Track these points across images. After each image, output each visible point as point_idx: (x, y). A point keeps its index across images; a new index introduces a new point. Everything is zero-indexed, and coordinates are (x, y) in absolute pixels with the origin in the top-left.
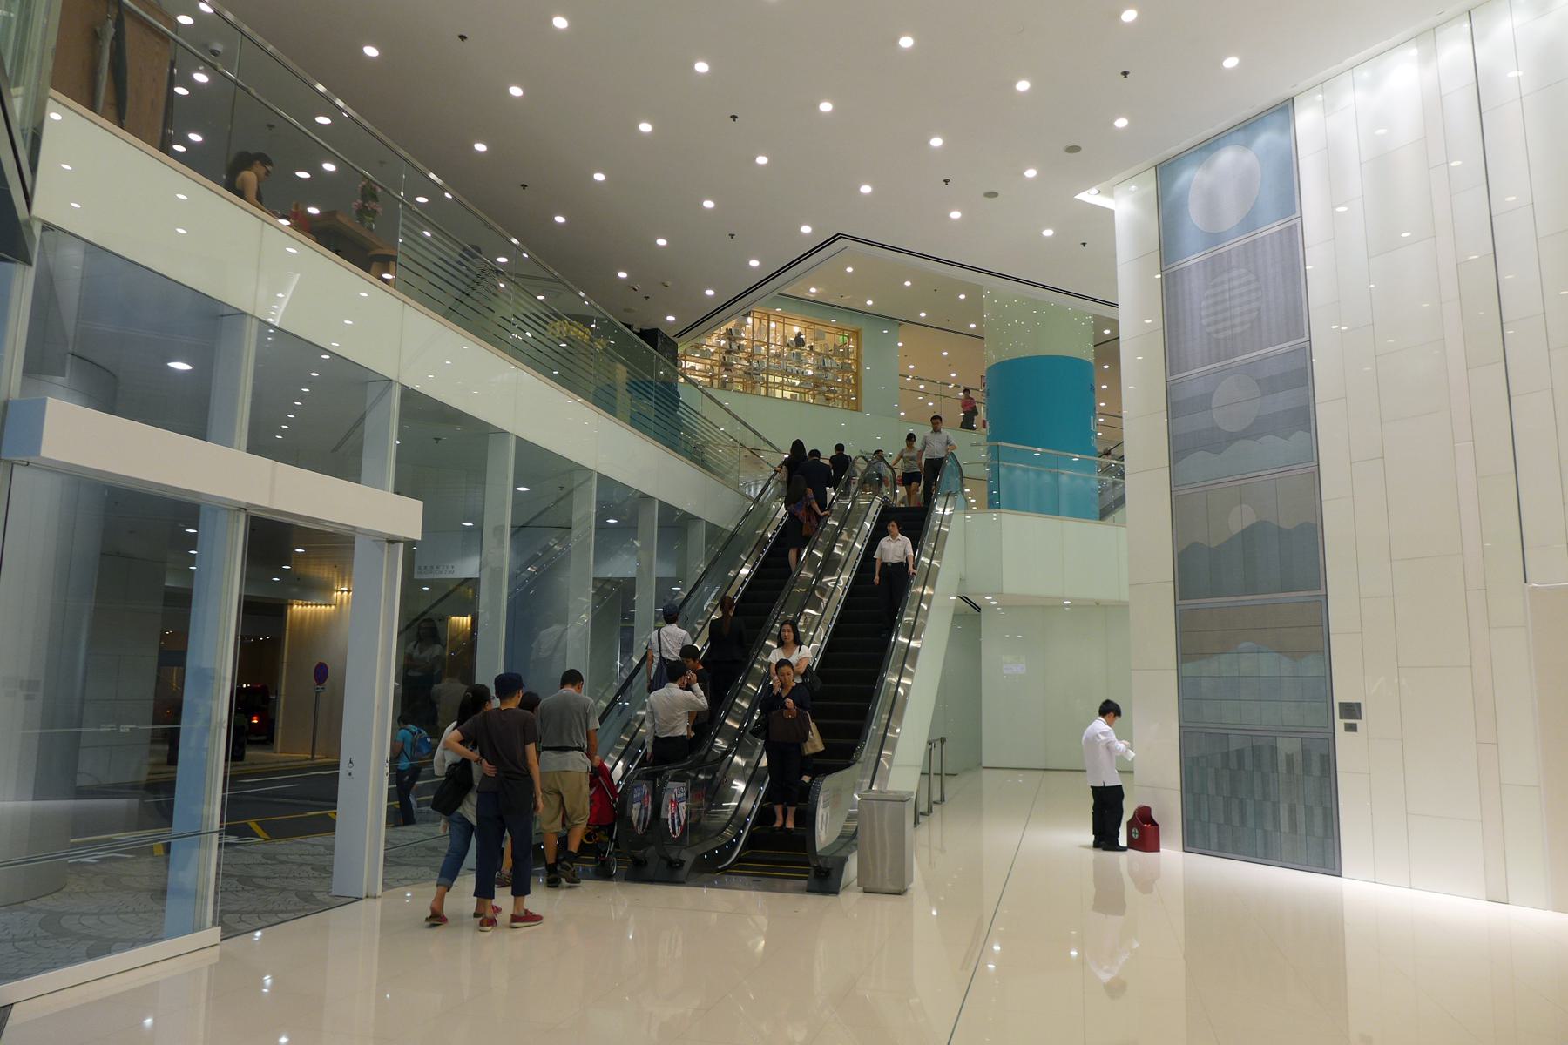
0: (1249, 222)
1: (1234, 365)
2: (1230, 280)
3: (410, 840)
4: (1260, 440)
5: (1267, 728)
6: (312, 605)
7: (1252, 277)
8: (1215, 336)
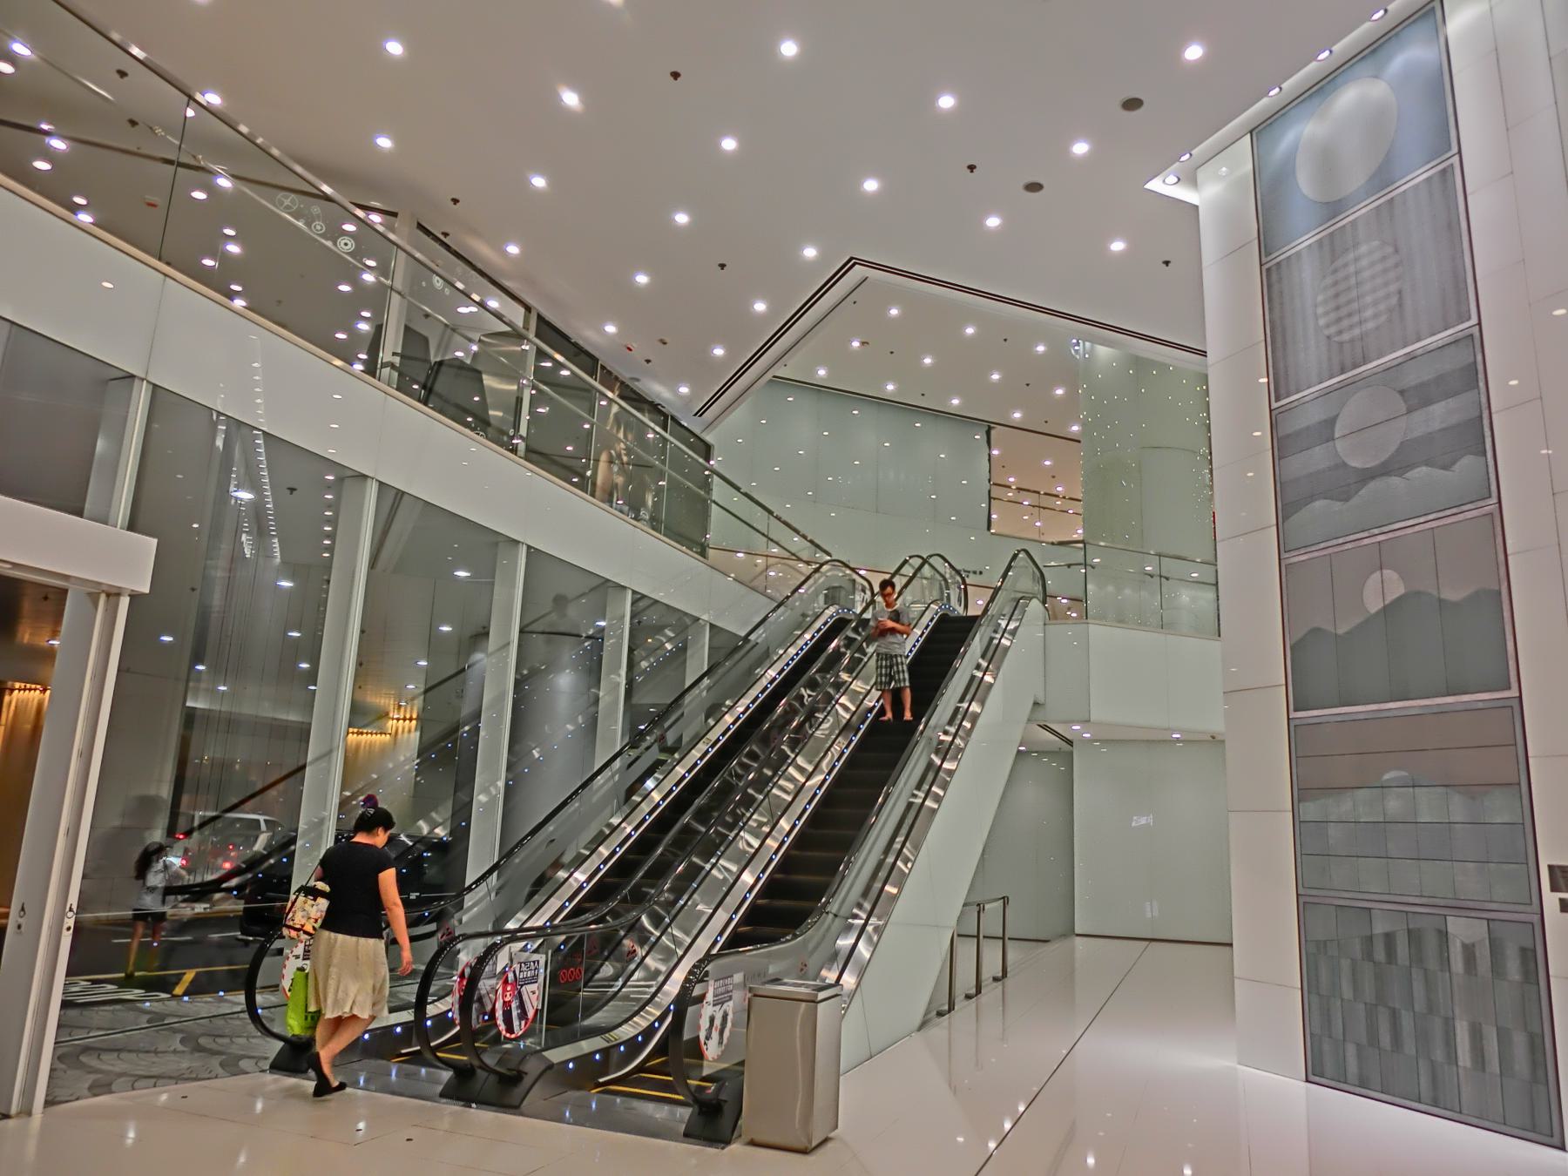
0: (1382, 178)
1: (1365, 375)
2: (1357, 260)
3: (238, 1018)
4: (1408, 475)
5: (1431, 901)
6: (367, 733)
7: (1390, 250)
8: (1336, 339)
